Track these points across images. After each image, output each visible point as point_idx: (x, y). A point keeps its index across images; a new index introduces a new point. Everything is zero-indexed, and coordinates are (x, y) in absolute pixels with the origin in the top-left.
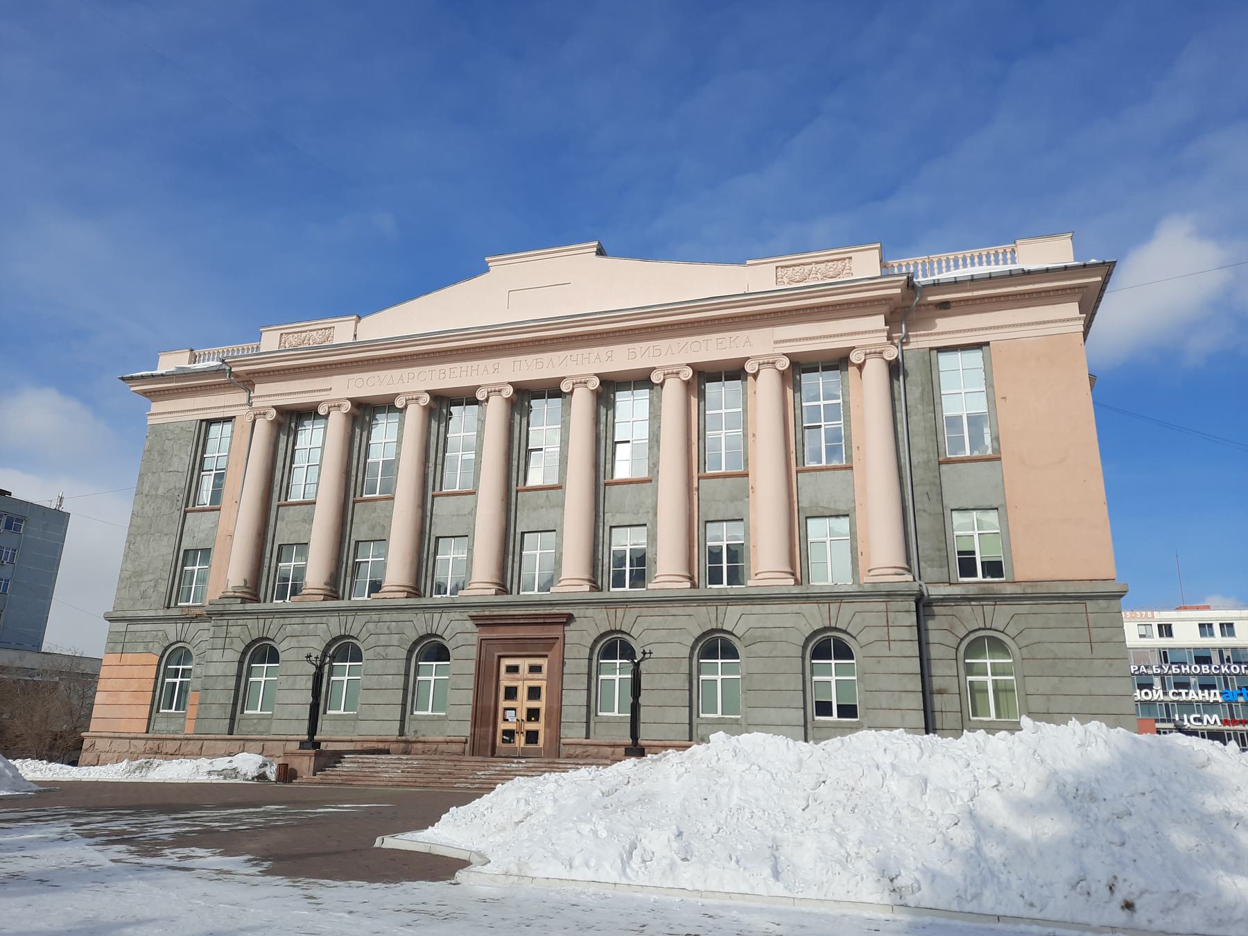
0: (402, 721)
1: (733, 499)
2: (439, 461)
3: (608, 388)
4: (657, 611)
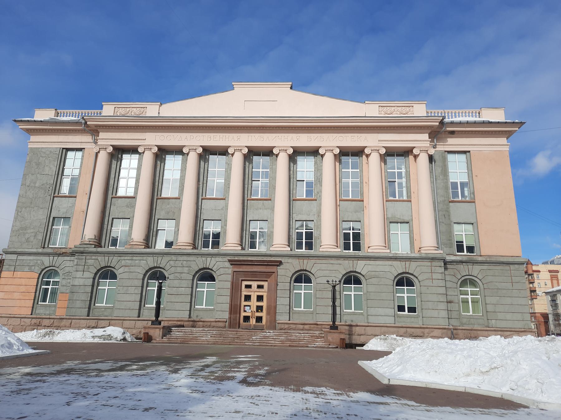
0: (140, 309)
1: (356, 212)
2: (205, 182)
4: (324, 261)
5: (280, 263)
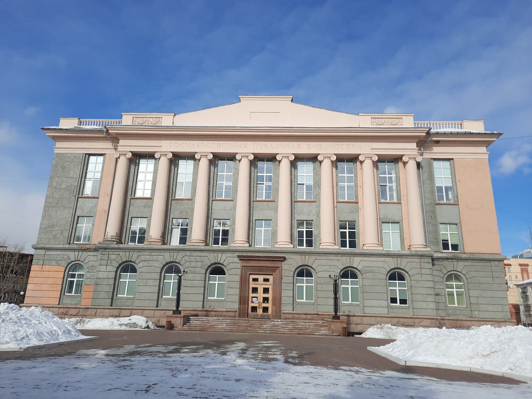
2: (215, 185)
3: (176, 158)
4: (324, 258)
5: (284, 259)
